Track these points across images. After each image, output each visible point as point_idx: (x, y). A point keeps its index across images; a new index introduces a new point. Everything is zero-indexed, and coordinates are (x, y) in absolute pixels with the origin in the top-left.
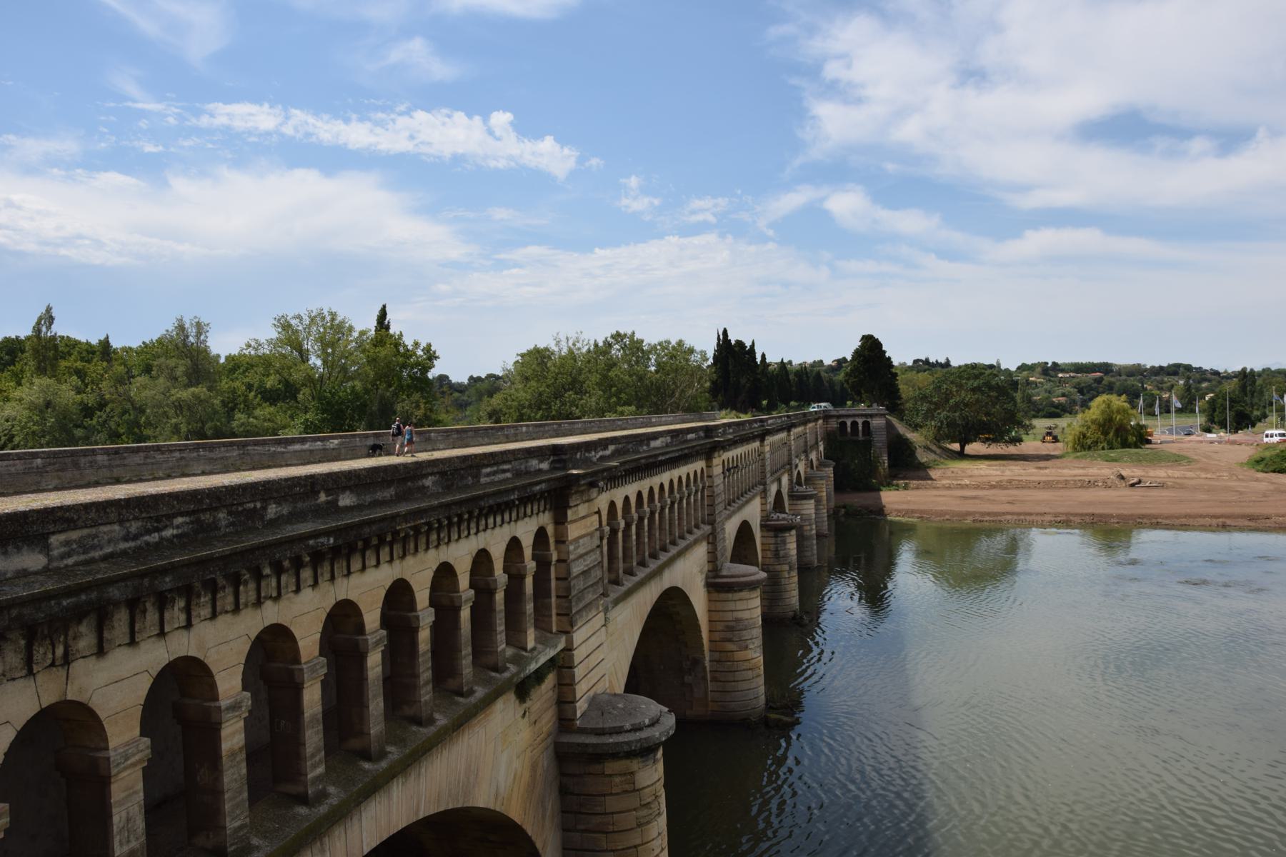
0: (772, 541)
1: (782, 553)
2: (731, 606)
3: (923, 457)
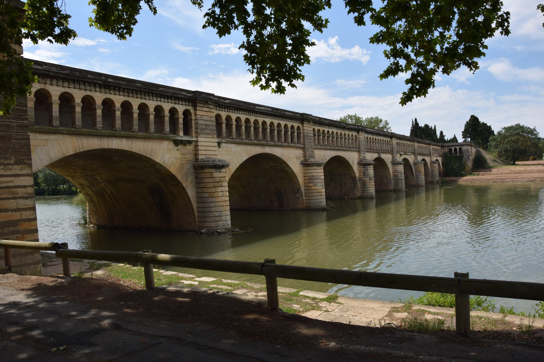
0: (363, 169)
1: (366, 174)
2: (310, 171)
3: (491, 164)
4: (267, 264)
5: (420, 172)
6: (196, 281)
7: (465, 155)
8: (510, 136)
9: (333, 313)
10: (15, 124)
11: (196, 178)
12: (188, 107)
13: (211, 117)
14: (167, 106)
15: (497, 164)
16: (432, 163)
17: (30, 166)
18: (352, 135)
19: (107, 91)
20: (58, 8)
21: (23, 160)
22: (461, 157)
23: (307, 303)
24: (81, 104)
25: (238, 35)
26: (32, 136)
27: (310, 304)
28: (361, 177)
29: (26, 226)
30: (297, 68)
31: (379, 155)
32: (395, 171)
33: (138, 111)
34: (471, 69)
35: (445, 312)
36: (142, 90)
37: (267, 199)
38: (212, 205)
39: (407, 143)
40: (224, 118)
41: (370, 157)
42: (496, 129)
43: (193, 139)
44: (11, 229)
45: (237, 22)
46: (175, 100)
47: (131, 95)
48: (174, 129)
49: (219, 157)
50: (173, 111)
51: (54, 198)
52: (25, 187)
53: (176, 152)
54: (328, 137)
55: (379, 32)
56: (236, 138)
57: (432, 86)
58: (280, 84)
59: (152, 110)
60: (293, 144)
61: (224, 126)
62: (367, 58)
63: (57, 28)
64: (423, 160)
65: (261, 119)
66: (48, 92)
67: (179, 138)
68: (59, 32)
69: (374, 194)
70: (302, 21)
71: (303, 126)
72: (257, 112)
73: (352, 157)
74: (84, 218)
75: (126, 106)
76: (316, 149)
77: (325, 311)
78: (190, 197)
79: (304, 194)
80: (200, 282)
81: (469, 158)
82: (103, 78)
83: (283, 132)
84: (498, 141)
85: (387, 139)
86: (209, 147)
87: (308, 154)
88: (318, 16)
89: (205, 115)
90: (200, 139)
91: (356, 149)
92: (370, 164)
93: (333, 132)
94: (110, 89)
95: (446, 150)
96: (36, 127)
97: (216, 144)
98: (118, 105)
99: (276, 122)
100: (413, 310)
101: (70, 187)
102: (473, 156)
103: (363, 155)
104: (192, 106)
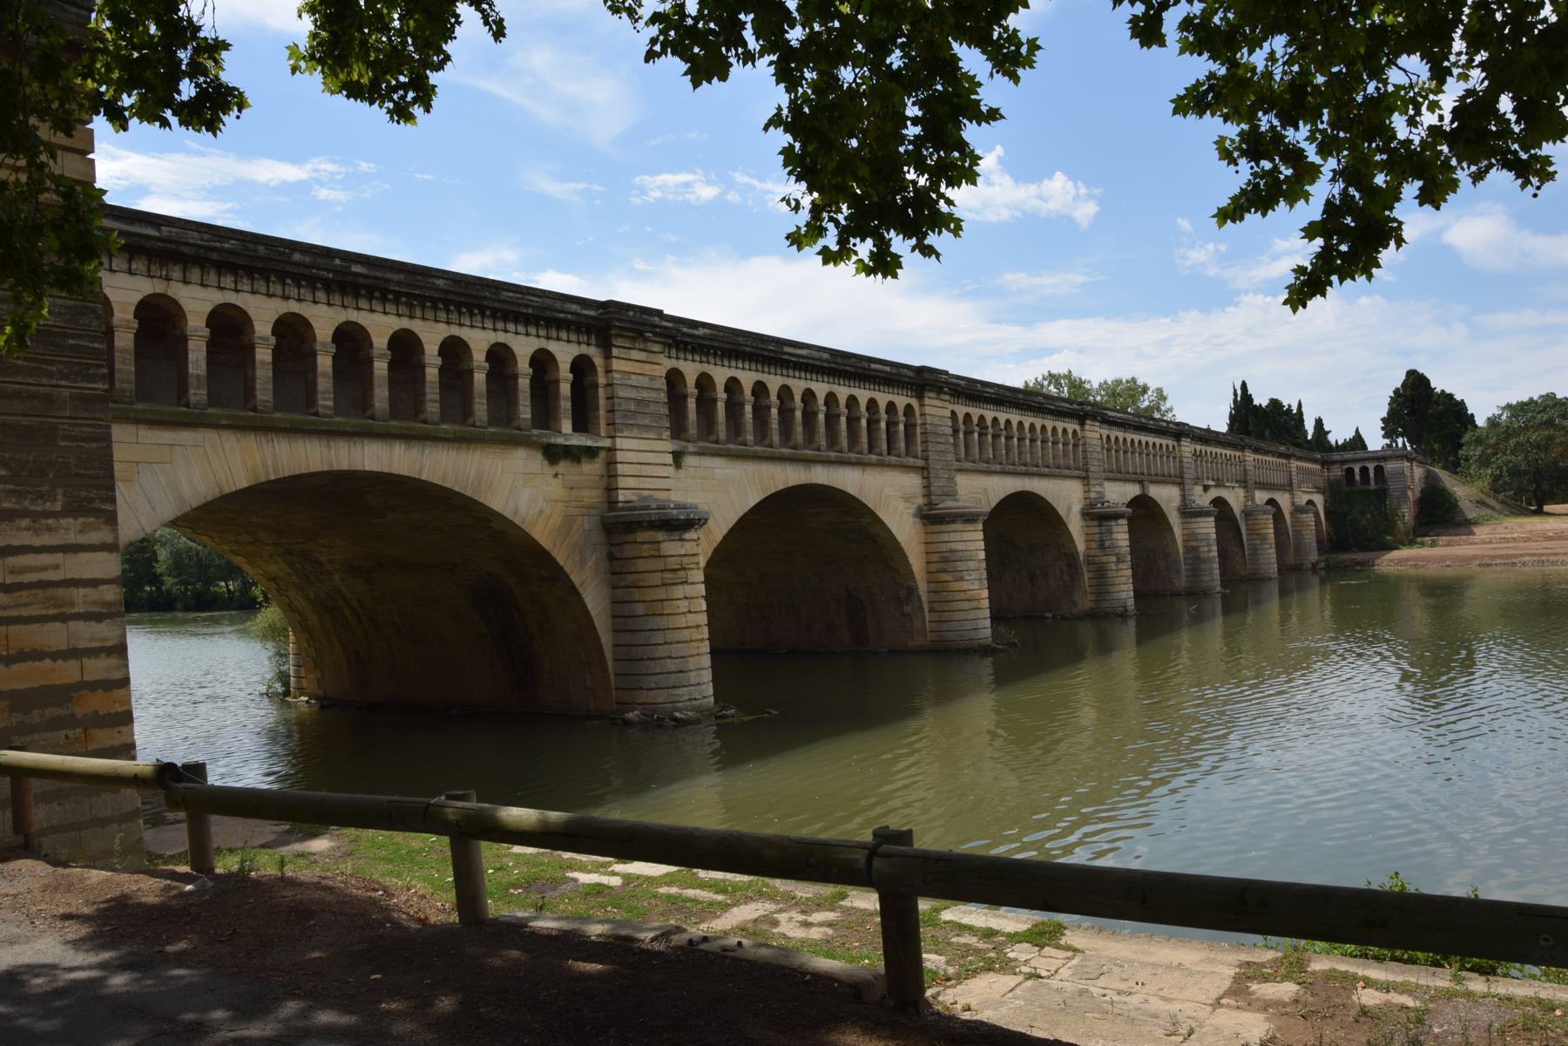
0: (1096, 530)
2: (945, 537)
3: (1471, 513)
4: (885, 848)
5: (1263, 538)
6: (614, 874)
7: (1393, 486)
8: (1526, 428)
9: (1054, 983)
10: (66, 393)
11: (611, 558)
12: (584, 350)
13: (652, 378)
14: (524, 346)
15: (1489, 512)
16: (1297, 510)
17: (111, 519)
18: (1065, 430)
19: (348, 300)
20: (190, 19)
21: (91, 500)
22: (1382, 494)
23: (968, 949)
24: (273, 340)
25: (755, 88)
26: (119, 432)
27: (977, 951)
28: (1093, 552)
29: (97, 702)
30: (942, 196)
31: (1143, 487)
32: (1190, 537)
33: (439, 361)
34: (1526, 183)
35: (1422, 982)
36: (451, 297)
37: (818, 624)
38: (658, 638)
39: (1224, 451)
40: (691, 380)
41: (1119, 493)
42: (1482, 409)
43: (601, 444)
44: (51, 712)
45: (753, 44)
46: (547, 327)
47: (418, 313)
48: (545, 414)
49: (677, 497)
50: (542, 361)
51: (205, 620)
52: (94, 583)
53: (553, 480)
54: (996, 437)
55: (1202, 78)
56: (729, 441)
57: (1392, 243)
58: (883, 247)
59: (479, 356)
60: (893, 459)
61: (692, 404)
62: (1091, 208)
63: (187, 81)
64: (1271, 502)
65: (798, 385)
66: (175, 302)
67: (560, 441)
68: (193, 94)
69: (1131, 602)
70: (955, 45)
71: (922, 405)
72: (788, 362)
73: (1066, 496)
74: (283, 677)
75: (404, 345)
76: (959, 470)
77: (1030, 976)
78: (593, 614)
79: (926, 606)
80: (628, 878)
81: (1406, 496)
82: (337, 262)
83: (864, 423)
84: (1492, 446)
85: (1164, 442)
86: (647, 466)
87: (937, 485)
88: (1006, 29)
89: (636, 371)
90: (620, 443)
91: (1076, 473)
92: (1117, 516)
93: (1008, 422)
94: (357, 296)
95: (1337, 472)
96: (140, 406)
97: (669, 459)
98: (380, 342)
99: (843, 392)
100: (1314, 973)
101: (247, 585)
102: (1418, 489)
103: (1098, 489)
104: (597, 346)
